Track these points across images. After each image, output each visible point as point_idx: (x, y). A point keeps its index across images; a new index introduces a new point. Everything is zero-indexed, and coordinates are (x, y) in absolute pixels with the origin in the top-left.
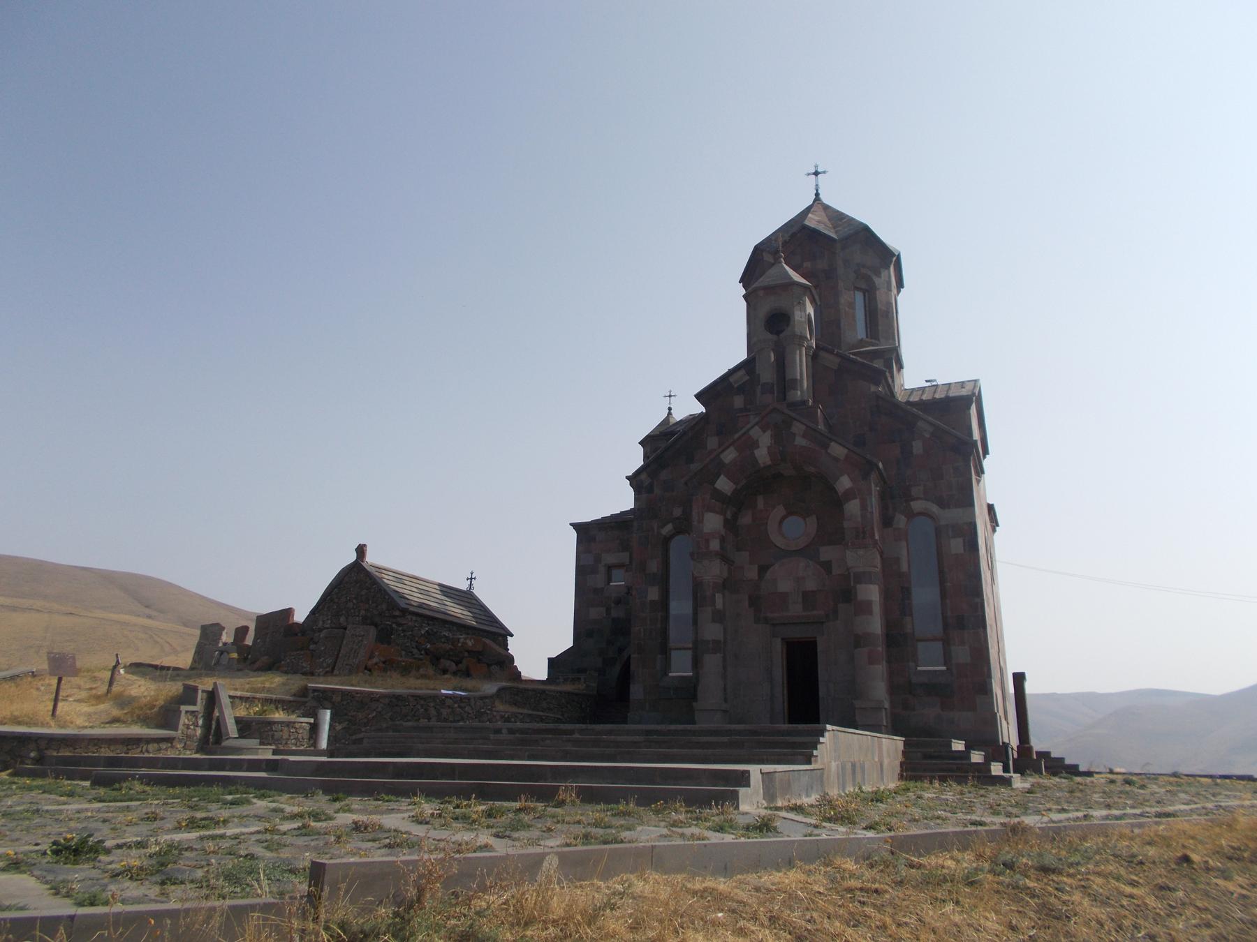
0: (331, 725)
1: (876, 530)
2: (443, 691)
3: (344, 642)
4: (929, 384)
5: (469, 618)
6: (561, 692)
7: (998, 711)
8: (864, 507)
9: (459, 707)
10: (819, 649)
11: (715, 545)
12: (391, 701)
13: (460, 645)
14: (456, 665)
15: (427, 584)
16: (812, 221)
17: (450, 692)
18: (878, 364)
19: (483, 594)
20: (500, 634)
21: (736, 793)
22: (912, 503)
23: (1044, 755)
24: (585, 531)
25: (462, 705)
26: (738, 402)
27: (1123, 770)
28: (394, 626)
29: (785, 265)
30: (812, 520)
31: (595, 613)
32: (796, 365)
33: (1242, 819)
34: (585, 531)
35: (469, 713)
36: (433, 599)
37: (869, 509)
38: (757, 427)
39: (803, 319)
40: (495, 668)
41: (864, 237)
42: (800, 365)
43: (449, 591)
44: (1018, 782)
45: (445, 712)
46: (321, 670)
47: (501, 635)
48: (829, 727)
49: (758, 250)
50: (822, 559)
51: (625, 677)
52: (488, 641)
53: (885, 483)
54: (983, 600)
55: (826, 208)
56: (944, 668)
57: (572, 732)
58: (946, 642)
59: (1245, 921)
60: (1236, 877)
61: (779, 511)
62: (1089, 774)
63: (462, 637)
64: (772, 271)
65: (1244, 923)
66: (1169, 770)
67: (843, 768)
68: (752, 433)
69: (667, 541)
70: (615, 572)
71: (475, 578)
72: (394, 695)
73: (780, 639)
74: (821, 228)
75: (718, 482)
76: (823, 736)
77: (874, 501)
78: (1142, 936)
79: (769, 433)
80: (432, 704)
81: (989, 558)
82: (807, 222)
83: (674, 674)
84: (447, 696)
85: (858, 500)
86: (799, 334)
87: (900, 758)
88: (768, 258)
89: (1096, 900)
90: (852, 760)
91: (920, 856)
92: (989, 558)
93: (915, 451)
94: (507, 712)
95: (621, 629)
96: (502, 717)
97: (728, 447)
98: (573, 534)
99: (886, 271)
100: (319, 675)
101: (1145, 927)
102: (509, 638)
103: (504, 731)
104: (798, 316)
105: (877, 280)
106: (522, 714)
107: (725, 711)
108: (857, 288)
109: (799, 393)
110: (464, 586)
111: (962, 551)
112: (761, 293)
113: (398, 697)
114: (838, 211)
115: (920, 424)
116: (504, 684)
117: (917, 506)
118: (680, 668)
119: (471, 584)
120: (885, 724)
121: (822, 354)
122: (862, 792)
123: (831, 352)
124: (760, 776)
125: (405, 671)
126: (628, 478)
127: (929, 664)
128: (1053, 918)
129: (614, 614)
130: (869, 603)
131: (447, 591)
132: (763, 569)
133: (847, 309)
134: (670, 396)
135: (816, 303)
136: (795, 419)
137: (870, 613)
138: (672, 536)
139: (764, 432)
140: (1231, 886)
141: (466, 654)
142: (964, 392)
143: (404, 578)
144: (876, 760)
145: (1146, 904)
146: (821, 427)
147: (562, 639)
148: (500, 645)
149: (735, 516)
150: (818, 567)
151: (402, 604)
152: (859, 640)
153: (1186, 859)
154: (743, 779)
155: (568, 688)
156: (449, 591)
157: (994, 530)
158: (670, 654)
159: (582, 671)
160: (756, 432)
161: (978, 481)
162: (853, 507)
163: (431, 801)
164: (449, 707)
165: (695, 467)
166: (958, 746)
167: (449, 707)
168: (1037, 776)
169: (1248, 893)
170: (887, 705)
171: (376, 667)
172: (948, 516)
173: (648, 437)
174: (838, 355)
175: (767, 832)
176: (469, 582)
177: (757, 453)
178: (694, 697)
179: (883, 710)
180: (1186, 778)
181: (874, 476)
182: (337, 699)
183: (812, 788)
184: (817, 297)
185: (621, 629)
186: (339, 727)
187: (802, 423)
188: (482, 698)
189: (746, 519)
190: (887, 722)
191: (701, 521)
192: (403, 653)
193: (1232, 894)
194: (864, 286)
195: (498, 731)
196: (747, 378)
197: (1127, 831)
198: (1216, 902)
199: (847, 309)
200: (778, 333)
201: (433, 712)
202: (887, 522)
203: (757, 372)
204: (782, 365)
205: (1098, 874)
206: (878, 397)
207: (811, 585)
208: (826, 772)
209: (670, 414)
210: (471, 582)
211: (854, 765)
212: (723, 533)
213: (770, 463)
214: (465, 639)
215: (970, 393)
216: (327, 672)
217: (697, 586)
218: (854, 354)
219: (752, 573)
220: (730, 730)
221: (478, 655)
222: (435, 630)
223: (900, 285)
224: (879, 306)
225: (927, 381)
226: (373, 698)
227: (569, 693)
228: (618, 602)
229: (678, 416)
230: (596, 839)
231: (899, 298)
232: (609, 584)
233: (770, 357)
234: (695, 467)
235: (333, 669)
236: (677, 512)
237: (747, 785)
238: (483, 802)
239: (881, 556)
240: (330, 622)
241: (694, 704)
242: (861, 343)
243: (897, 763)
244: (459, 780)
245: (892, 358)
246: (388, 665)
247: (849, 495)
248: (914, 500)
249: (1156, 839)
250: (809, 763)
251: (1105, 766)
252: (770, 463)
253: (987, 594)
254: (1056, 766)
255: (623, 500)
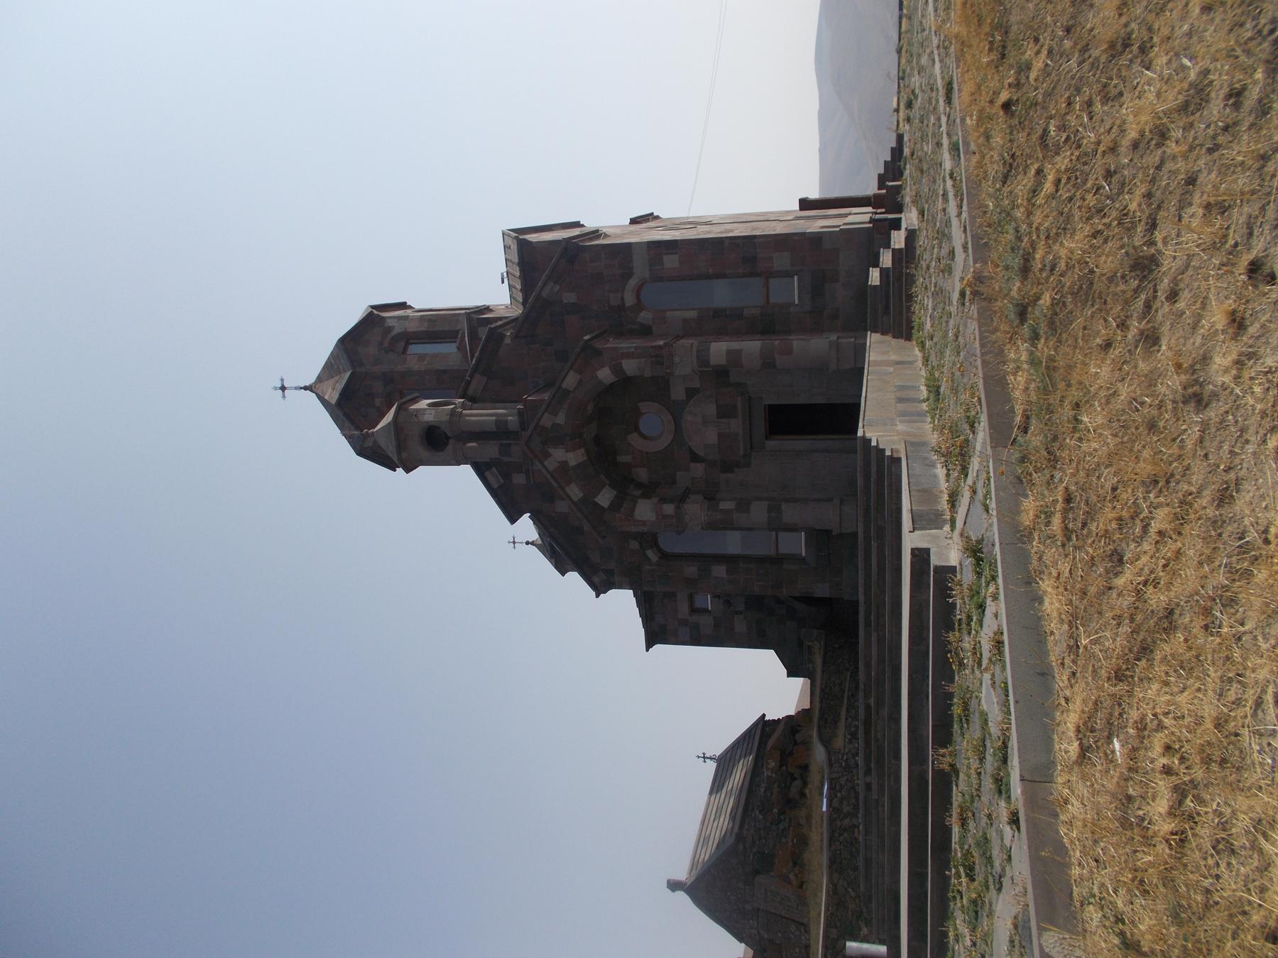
0: (862, 941)
1: (654, 344)
2: (824, 809)
3: (773, 911)
4: (506, 280)
5: (745, 763)
6: (823, 671)
7: (839, 226)
8: (629, 356)
9: (840, 791)
10: (775, 402)
11: (669, 509)
12: (836, 871)
13: (774, 775)
14: (795, 779)
15: (710, 808)
16: (333, 396)
17: (825, 800)
18: (483, 333)
19: (719, 746)
20: (763, 727)
21: (937, 569)
22: (627, 305)
23: (882, 180)
24: (654, 636)
25: (838, 787)
26: (519, 479)
27: (895, 100)
28: (754, 850)
29: (376, 429)
30: (643, 406)
31: (740, 626)
32: (479, 420)
33: (956, 29)
34: (654, 636)
35: (847, 780)
36: (726, 803)
37: (633, 350)
38: (546, 463)
39: (433, 412)
40: (798, 737)
41: (351, 343)
42: (482, 415)
43: (716, 784)
44: (910, 218)
45: (846, 808)
46: (803, 937)
47: (763, 729)
48: (860, 433)
49: (361, 452)
50: (684, 397)
51: (808, 600)
52: (770, 743)
53: (605, 332)
54: (726, 237)
55: (320, 379)
56: (796, 277)
57: (868, 707)
58: (769, 275)
59: (1081, 59)
60: (1027, 56)
61: (634, 439)
62: (900, 138)
63: (766, 773)
64: (383, 442)
65: (1084, 61)
66: (896, 56)
67: (903, 414)
68: (551, 469)
69: (664, 556)
70: (698, 603)
71: (704, 754)
72: (830, 867)
73: (766, 442)
74: (340, 386)
75: (603, 505)
76: (870, 440)
77: (626, 345)
78: (1108, 185)
79: (552, 450)
80: (839, 823)
81: (685, 227)
82: (333, 401)
83: (796, 297)
84: (830, 805)
85: (623, 361)
86: (448, 417)
87: (888, 338)
88: (369, 443)
89: (1064, 229)
90: (894, 402)
91: (1012, 410)
92: (685, 227)
93: (572, 301)
94: (845, 737)
95: (755, 603)
96: (850, 742)
97: (565, 493)
98: (658, 648)
99: (388, 321)
100: (809, 940)
101: (1097, 179)
102: (767, 718)
103: (868, 780)
104: (430, 417)
105: (397, 331)
106: (847, 719)
107: (842, 502)
108: (405, 351)
109: (510, 418)
110: (712, 766)
111: (677, 256)
112: (404, 455)
113: (832, 862)
114: (324, 368)
115: (544, 294)
116: (815, 734)
117: (629, 300)
118: (797, 544)
119: (711, 758)
120: (853, 340)
121: (470, 392)
122: (928, 400)
123: (469, 383)
124: (917, 532)
125: (803, 841)
126: (597, 596)
127: (792, 292)
128: (1091, 289)
129: (741, 607)
130: (729, 352)
131: (717, 785)
132: (695, 458)
133: (425, 362)
134: (514, 542)
135: (418, 397)
136: (538, 423)
137: (739, 352)
138: (660, 550)
139: (550, 455)
140: (1038, 65)
141: (784, 768)
142: (514, 247)
143: (703, 835)
144: (891, 369)
145: (1067, 170)
146: (546, 396)
147: (766, 662)
148: (774, 731)
149: (639, 485)
150: (692, 401)
151: (731, 840)
152: (768, 363)
153: (1007, 106)
154: (921, 556)
155: (818, 660)
156: (716, 784)
157: (657, 217)
158: (782, 554)
159: (801, 644)
160: (551, 464)
161: (606, 236)
162: (630, 367)
163: (952, 913)
164: (841, 803)
165: (586, 527)
166: (875, 277)
167: (841, 803)
168: (903, 192)
169: (1046, 47)
170: (834, 337)
171: (799, 875)
172: (640, 268)
173: (557, 567)
174: (472, 376)
175: (982, 553)
176: (708, 761)
177: (572, 463)
178: (828, 532)
179: (840, 340)
180: (901, 43)
181: (598, 345)
182: (834, 933)
183: (926, 458)
184: (413, 396)
185: (755, 603)
186: (865, 931)
187: (541, 417)
188: (831, 765)
189: (642, 474)
190: (852, 337)
191: (644, 523)
192: (784, 840)
193: (1047, 65)
194: (402, 344)
195: (868, 787)
196: (494, 469)
197: (975, 159)
198: (1059, 88)
199: (425, 362)
200: (448, 438)
201: (847, 822)
202: (646, 331)
203: (488, 460)
204: (481, 435)
205: (1029, 214)
206: (516, 337)
207: (711, 409)
208: (908, 438)
209: (533, 543)
210: (708, 758)
211: (900, 400)
212: (655, 500)
213: (583, 450)
214: (768, 769)
215: (515, 242)
216: (806, 932)
217: (711, 526)
218: (472, 357)
219: (698, 470)
220: (865, 537)
221: (785, 755)
222: (759, 803)
223: (403, 306)
224: (423, 329)
225: (503, 282)
226: (834, 891)
227: (824, 663)
228: (728, 603)
229: (534, 535)
230: (999, 769)
231: (417, 307)
232: (710, 612)
233: (471, 447)
234: (586, 527)
235: (802, 924)
236: (634, 545)
237: (927, 551)
238: (953, 854)
239: (682, 338)
240: (751, 921)
241: (834, 533)
242: (461, 348)
243: (894, 342)
244: (927, 868)
245: (477, 317)
246: (797, 861)
247: (617, 370)
248: (624, 304)
249: (982, 130)
250: (899, 460)
251: (891, 116)
252: (583, 450)
253: (721, 232)
254: (893, 170)
255: (623, 601)
